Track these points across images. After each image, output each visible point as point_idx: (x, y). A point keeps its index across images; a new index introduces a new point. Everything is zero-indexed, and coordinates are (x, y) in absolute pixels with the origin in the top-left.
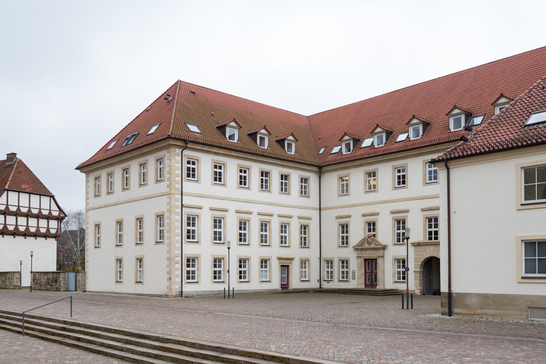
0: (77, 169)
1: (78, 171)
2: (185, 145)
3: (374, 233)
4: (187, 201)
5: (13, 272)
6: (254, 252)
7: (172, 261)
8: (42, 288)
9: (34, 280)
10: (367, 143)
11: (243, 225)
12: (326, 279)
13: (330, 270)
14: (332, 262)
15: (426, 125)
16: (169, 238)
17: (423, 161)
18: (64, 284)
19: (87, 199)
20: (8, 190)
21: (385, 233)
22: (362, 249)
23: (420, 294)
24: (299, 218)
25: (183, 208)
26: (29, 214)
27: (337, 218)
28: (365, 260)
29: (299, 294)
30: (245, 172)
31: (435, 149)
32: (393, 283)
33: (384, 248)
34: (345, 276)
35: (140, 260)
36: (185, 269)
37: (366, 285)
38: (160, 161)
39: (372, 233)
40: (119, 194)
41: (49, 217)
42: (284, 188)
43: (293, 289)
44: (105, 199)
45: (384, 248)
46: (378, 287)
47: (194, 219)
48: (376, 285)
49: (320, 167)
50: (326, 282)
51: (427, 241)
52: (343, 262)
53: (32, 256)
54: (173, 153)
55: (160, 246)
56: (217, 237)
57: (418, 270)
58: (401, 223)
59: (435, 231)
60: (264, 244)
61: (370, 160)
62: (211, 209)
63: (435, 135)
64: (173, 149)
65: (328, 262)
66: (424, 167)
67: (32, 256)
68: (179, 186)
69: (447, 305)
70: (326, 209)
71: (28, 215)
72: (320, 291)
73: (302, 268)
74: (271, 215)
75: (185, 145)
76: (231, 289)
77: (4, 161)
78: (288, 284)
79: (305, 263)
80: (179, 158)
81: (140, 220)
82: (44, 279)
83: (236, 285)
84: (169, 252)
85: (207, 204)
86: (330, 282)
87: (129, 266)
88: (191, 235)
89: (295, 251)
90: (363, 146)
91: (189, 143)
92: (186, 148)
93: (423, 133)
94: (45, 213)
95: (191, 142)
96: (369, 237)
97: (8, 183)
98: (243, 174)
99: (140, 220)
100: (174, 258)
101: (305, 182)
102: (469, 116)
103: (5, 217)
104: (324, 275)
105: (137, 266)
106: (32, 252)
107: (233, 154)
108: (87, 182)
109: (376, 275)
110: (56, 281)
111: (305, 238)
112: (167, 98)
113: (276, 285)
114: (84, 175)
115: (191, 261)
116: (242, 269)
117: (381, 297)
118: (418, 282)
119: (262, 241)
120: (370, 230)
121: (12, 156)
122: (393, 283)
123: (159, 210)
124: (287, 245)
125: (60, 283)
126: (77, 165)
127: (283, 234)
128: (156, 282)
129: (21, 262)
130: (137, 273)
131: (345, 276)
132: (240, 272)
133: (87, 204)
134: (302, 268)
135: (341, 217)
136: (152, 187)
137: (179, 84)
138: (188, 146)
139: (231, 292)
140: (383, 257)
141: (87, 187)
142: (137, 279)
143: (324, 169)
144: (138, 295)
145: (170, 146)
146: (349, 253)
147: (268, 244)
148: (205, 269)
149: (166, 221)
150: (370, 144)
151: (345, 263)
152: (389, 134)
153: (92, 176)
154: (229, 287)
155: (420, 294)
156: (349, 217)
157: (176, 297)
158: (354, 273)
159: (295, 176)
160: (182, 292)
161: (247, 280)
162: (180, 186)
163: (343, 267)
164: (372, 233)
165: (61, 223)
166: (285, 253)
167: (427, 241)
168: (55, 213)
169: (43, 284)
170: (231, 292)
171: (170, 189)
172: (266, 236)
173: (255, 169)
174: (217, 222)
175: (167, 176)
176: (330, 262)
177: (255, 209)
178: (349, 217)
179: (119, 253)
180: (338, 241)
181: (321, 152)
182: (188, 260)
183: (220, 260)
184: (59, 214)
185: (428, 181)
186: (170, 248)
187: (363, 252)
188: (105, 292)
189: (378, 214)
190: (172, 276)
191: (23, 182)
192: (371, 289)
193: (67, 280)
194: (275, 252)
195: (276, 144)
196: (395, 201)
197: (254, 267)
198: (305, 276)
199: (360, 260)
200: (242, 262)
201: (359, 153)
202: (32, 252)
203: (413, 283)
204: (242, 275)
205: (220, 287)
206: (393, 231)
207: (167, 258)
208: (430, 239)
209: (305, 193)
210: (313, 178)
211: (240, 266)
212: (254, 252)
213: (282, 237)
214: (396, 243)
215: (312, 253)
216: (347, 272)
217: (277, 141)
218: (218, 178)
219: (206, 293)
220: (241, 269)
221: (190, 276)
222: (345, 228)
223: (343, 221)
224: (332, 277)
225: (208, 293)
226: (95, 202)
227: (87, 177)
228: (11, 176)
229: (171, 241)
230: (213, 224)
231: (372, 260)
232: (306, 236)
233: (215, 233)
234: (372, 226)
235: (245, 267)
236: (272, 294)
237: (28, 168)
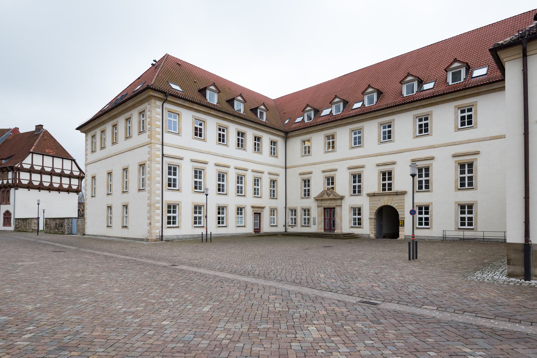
0: (77, 129)
1: (79, 131)
2: (165, 98)
3: (333, 186)
4: (167, 151)
5: (31, 218)
6: (231, 201)
7: (152, 207)
8: (52, 231)
9: (46, 224)
10: (326, 112)
11: (221, 177)
12: (290, 224)
13: (294, 217)
14: (295, 211)
15: (380, 93)
16: (150, 185)
17: (378, 123)
18: (68, 228)
19: (86, 155)
20: (33, 153)
21: (343, 186)
22: (322, 200)
23: (374, 238)
24: (269, 174)
25: (164, 158)
26: (53, 172)
27: (300, 174)
28: (325, 209)
29: (270, 238)
30: (223, 131)
31: (390, 112)
32: (350, 228)
33: (342, 198)
34: (307, 222)
35: (126, 206)
36: (166, 215)
37: (325, 229)
38: (142, 113)
39: (331, 186)
40: (110, 149)
41: (71, 176)
42: (257, 148)
43: (264, 233)
44: (100, 154)
45: (342, 198)
46: (336, 231)
47: (175, 169)
48: (335, 230)
49: (286, 133)
50: (290, 227)
51: (381, 192)
52: (305, 211)
53: (38, 204)
54: (153, 105)
55: (142, 193)
56: (197, 186)
57: (373, 217)
58: (357, 178)
59: (388, 184)
60: (240, 194)
61: (329, 125)
62: (192, 161)
63: (388, 100)
64: (153, 101)
65: (292, 211)
66: (379, 128)
67: (38, 204)
68: (160, 137)
69: (522, 262)
70: (290, 167)
71: (42, 172)
72: (286, 235)
73: (271, 215)
74: (246, 170)
75: (165, 98)
76: (209, 233)
77: (34, 132)
78: (260, 229)
79: (274, 211)
80: (160, 110)
81: (125, 170)
82: (53, 224)
83: (213, 228)
84: (149, 198)
85: (188, 156)
86: (294, 227)
87: (117, 211)
88: (172, 184)
89: (265, 201)
90: (323, 114)
91: (169, 96)
92: (165, 101)
93: (378, 100)
94: (68, 172)
95: (170, 95)
96: (328, 189)
97: (33, 147)
98: (222, 133)
99: (125, 170)
100: (155, 204)
101: (274, 145)
102: (421, 83)
103: (41, 176)
104: (289, 221)
105: (123, 212)
106: (39, 201)
107: (212, 112)
108: (86, 140)
109: (334, 222)
110: (62, 226)
111: (274, 191)
112: (155, 66)
113: (249, 229)
114: (84, 134)
115: (172, 208)
116: (221, 216)
117: (344, 240)
118: (373, 227)
119: (238, 192)
120: (328, 184)
121: (39, 127)
122: (350, 228)
123: (141, 160)
124: (259, 196)
125: (64, 227)
126: (78, 126)
127: (256, 187)
128: (138, 228)
129: (44, 210)
130: (123, 218)
131: (307, 222)
132: (219, 218)
133: (86, 160)
134: (271, 215)
135: (304, 174)
136: (137, 139)
137: (167, 57)
138: (169, 99)
139: (209, 236)
140: (341, 206)
141: (86, 145)
142: (123, 223)
143: (289, 135)
144: (124, 238)
145: (150, 97)
146: (310, 203)
147: (243, 194)
148: (185, 216)
149: (147, 169)
150: (328, 113)
151: (307, 211)
152: (346, 103)
153: (90, 134)
154: (207, 231)
155: (374, 238)
156: (311, 173)
157: (156, 241)
158: (314, 219)
159: (266, 139)
160: (162, 236)
161: (224, 225)
162: (160, 137)
163: (305, 215)
164: (331, 186)
165: (81, 181)
166: (258, 202)
167: (381, 192)
168: (77, 173)
169: (53, 228)
170: (209, 236)
171: (151, 139)
172: (242, 187)
173: (232, 129)
174: (198, 173)
175: (148, 126)
176: (294, 211)
177: (233, 163)
178: (311, 173)
179: (110, 200)
180: (301, 193)
181: (287, 122)
182: (169, 207)
183: (200, 207)
184: (80, 174)
185: (382, 141)
186: (151, 195)
187: (323, 202)
188: (98, 236)
189: (336, 170)
190: (152, 221)
191: (48, 148)
192: (330, 233)
193: (70, 225)
194: (249, 201)
195: (250, 112)
196: (352, 159)
197: (231, 213)
198: (274, 222)
199: (320, 209)
200: (221, 210)
201: (319, 120)
202: (39, 201)
203: (367, 228)
204: (221, 221)
205: (199, 232)
206: (350, 184)
207: (148, 204)
208: (384, 190)
209: (274, 154)
210: (280, 142)
211: (219, 213)
212: (231, 201)
213: (255, 189)
214: (352, 194)
215: (279, 203)
216: (309, 219)
217: (251, 110)
218: (198, 133)
219: (186, 237)
220: (219, 216)
221: (171, 221)
222: (307, 182)
223: (306, 177)
224: (295, 223)
225: (188, 237)
226: (92, 157)
227: (86, 136)
228: (37, 142)
229: (151, 188)
230: (194, 174)
231: (330, 209)
232: (275, 189)
233: (196, 182)
234: (331, 181)
235: (223, 213)
236: (247, 236)
237: (52, 137)
